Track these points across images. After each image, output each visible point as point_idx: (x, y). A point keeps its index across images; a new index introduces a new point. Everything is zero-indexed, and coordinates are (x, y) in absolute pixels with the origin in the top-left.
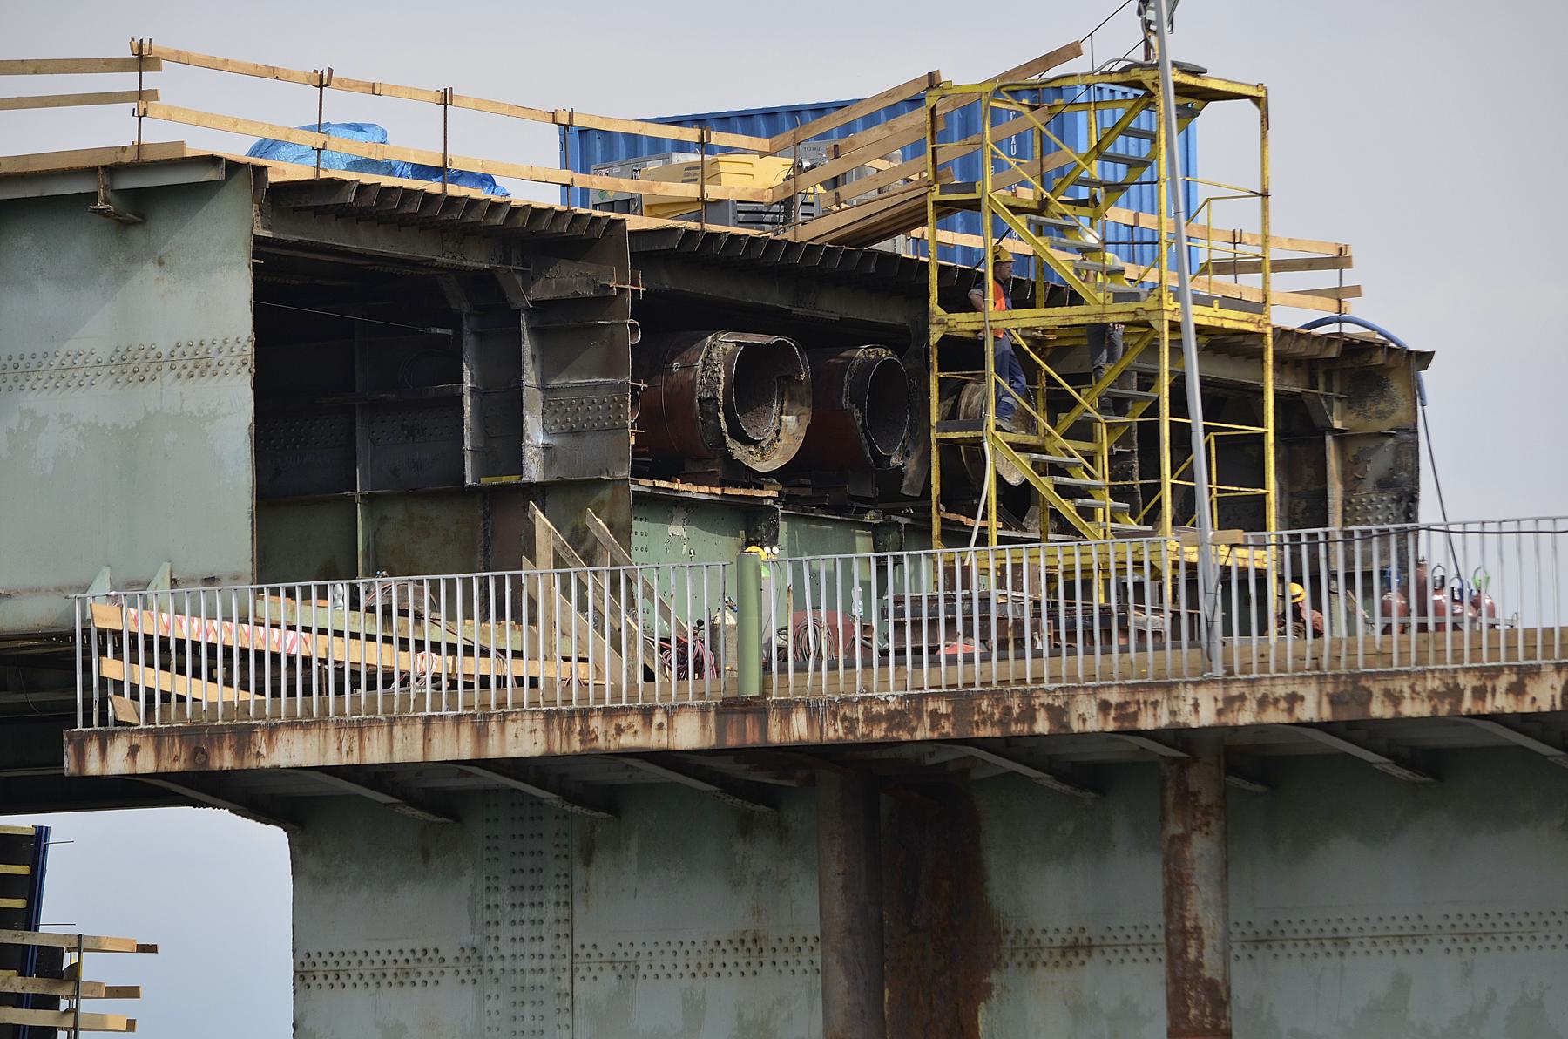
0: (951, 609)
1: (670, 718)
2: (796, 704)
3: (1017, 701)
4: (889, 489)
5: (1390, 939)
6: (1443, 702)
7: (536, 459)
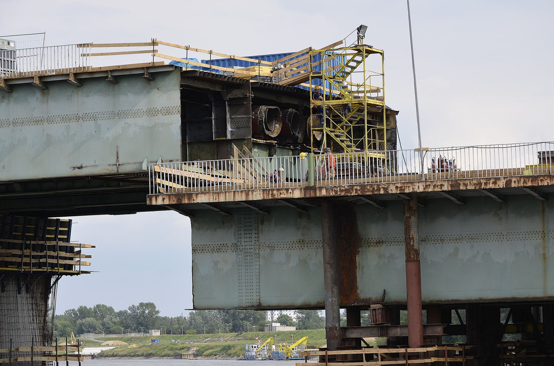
0: (343, 167)
1: (293, 191)
2: (323, 187)
3: (376, 186)
4: (295, 142)
5: (454, 240)
6: (477, 186)
7: (229, 134)
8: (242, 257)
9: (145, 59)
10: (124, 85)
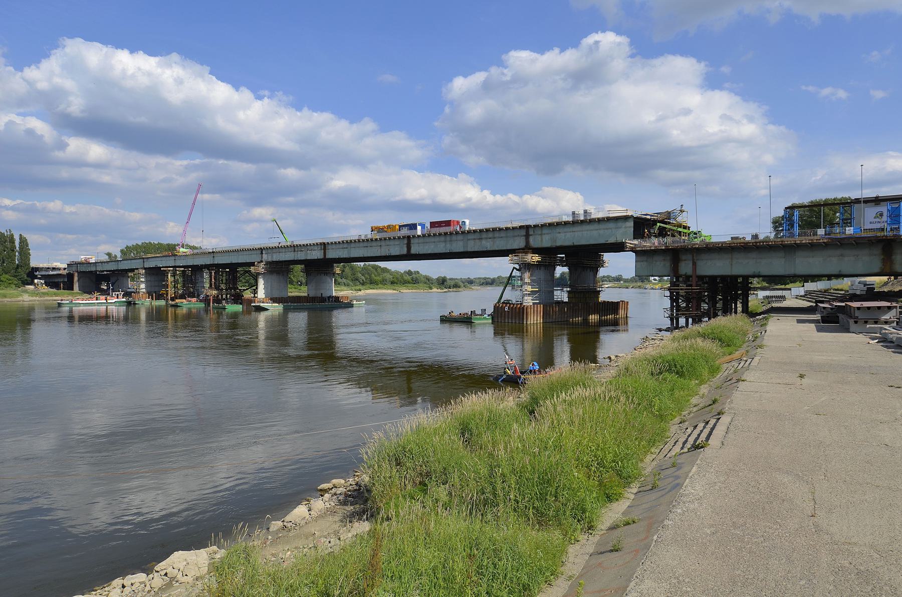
9: (625, 214)
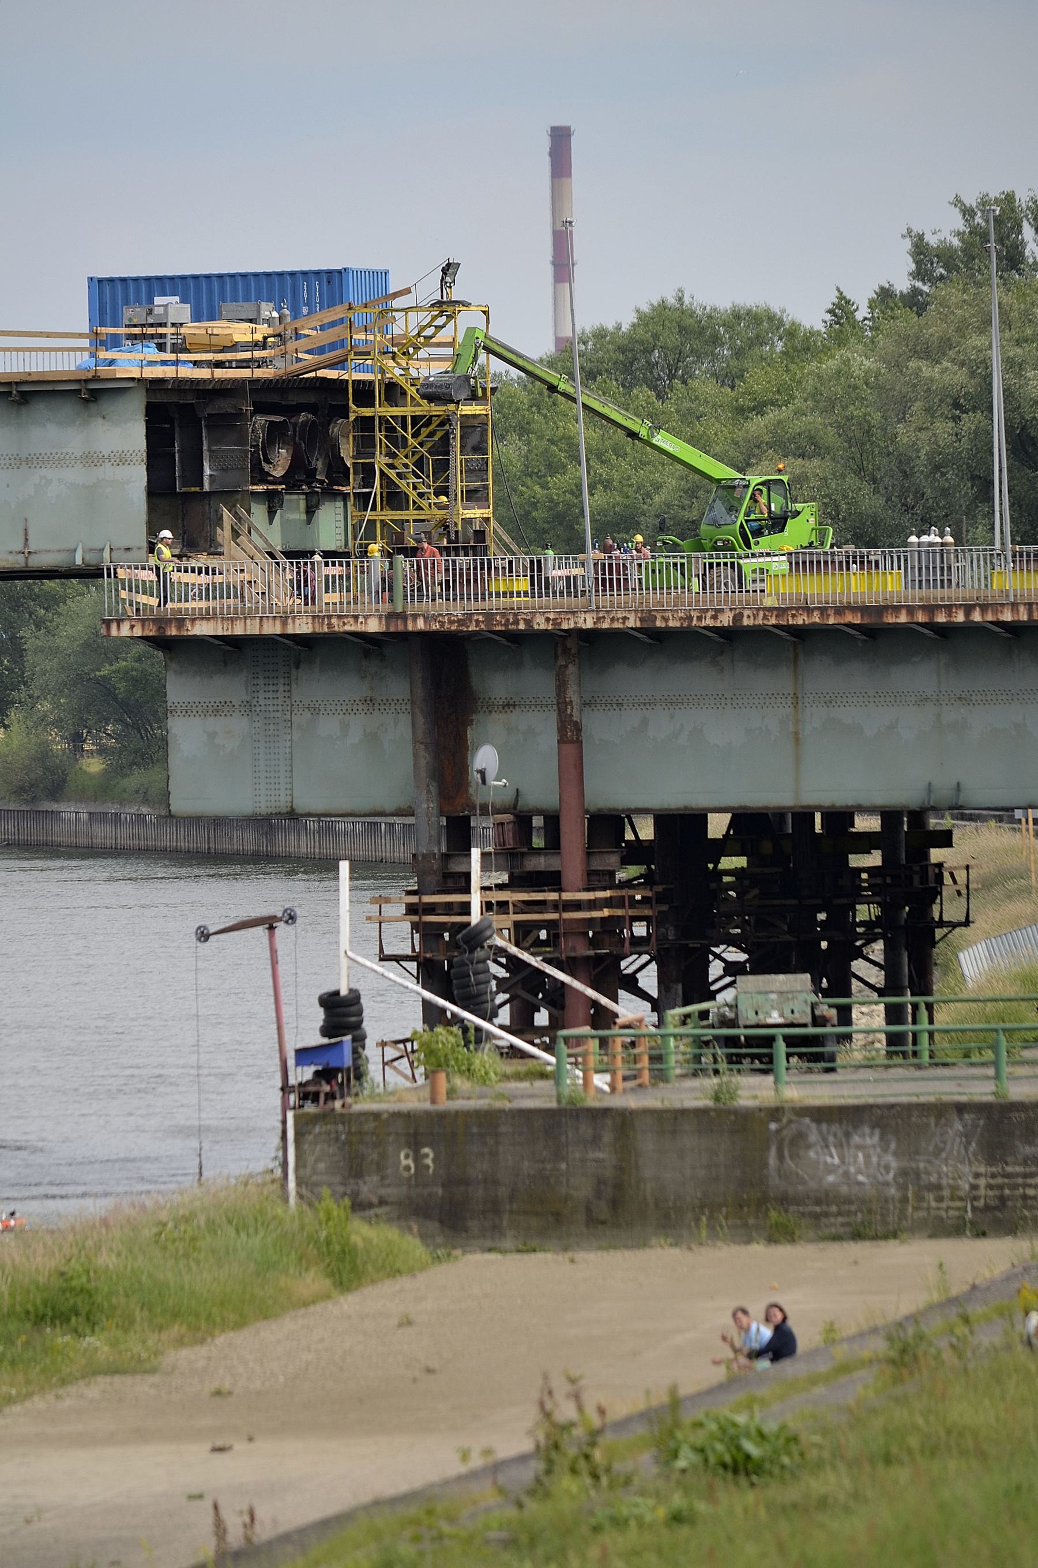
8: (259, 725)
10: (40, 409)
